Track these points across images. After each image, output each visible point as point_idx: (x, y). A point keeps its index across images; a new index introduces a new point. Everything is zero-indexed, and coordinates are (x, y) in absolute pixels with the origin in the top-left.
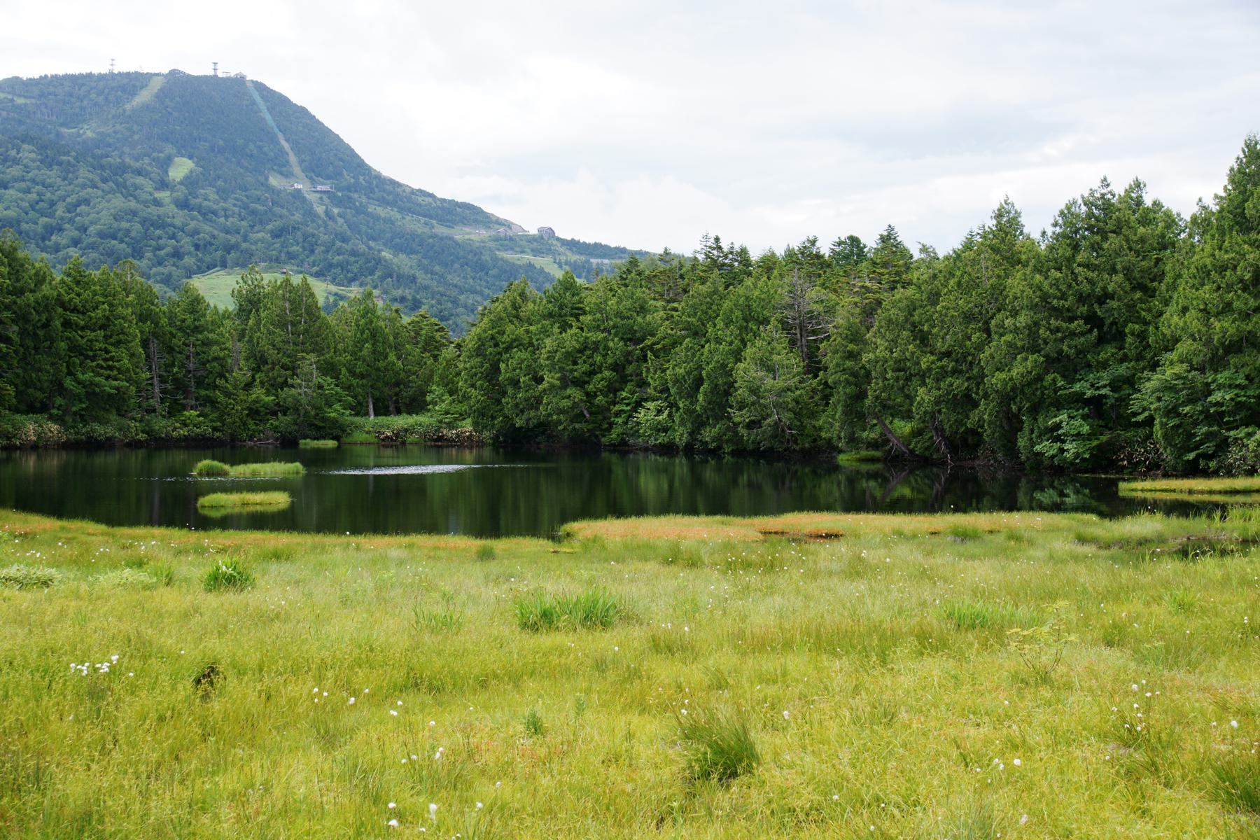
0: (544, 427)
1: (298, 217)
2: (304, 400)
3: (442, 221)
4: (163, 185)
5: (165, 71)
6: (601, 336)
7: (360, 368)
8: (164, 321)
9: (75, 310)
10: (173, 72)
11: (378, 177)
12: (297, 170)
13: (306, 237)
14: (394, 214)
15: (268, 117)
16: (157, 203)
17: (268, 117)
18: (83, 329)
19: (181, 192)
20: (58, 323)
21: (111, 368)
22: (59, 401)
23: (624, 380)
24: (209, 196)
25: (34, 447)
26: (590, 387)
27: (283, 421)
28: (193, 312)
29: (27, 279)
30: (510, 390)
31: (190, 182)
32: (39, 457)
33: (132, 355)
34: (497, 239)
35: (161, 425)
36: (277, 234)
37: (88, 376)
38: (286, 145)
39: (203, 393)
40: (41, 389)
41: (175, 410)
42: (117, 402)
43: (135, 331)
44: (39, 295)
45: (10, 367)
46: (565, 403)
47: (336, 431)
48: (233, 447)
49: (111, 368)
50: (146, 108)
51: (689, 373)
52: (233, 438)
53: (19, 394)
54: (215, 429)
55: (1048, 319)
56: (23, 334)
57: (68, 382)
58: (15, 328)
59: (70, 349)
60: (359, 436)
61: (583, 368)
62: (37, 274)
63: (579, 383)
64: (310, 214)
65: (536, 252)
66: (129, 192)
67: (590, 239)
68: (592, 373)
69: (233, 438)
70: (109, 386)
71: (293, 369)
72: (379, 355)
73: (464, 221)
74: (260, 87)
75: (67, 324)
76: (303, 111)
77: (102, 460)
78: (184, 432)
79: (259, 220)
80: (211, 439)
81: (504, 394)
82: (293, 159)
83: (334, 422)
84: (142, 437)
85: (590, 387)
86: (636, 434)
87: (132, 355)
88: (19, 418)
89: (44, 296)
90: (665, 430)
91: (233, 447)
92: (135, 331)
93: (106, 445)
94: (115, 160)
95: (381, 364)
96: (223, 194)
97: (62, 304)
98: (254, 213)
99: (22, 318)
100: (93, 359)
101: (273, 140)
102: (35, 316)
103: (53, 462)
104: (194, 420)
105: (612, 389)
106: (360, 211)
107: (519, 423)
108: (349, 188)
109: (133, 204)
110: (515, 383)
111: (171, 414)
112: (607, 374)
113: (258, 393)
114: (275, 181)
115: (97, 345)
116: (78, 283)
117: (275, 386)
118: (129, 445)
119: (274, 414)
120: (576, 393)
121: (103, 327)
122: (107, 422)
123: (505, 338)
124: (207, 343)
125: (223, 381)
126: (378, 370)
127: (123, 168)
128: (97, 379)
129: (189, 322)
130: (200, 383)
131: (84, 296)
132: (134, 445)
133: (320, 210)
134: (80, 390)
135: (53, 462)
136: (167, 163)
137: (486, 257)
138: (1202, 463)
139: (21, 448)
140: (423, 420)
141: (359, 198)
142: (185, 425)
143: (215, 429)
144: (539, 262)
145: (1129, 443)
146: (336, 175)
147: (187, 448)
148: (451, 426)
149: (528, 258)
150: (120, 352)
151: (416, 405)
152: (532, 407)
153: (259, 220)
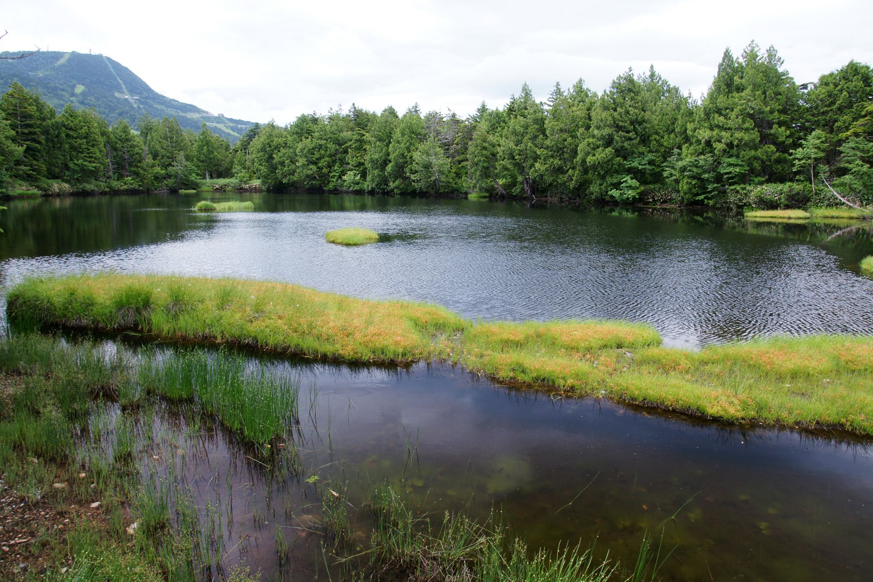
0: (293, 184)
1: (127, 108)
2: (180, 172)
3: (183, 111)
4: (73, 95)
5: (70, 51)
6: (323, 142)
7: (202, 158)
8: (112, 136)
9: (71, 129)
10: (73, 52)
11: (157, 94)
12: (125, 91)
13: (131, 116)
14: (164, 108)
15: (113, 70)
16: (72, 102)
17: (113, 70)
18: (76, 138)
19: (81, 98)
20: (64, 135)
21: (91, 157)
22: (67, 173)
23: (334, 162)
24: (91, 99)
25: (58, 195)
26: (320, 165)
27: (171, 182)
28: (125, 132)
29: (46, 111)
30: (280, 167)
31: (83, 94)
32: (61, 200)
33: (101, 151)
34: (203, 118)
35: (115, 184)
36: (120, 114)
37: (80, 161)
38: (121, 82)
39: (133, 169)
40: (58, 167)
41: (121, 177)
42: (94, 174)
43: (102, 140)
44: (53, 121)
45: (42, 156)
46: (309, 172)
47: (195, 186)
48: (148, 194)
49: (91, 157)
50: (63, 65)
51: (380, 158)
52: (148, 190)
53: (48, 169)
54: (140, 186)
55: (617, 132)
56: (47, 140)
57: (71, 165)
58: (43, 137)
59: (71, 148)
60: (204, 188)
61: (317, 155)
62: (51, 111)
63: (315, 163)
64: (132, 107)
65: (218, 122)
66: (60, 97)
67: (237, 119)
68: (320, 158)
69: (148, 190)
70: (91, 166)
71: (173, 158)
72: (211, 152)
73: (190, 111)
74: (108, 59)
75: (68, 136)
76: (126, 69)
77: (91, 201)
78: (125, 187)
79: (112, 110)
80: (139, 190)
81: (276, 169)
82: (123, 86)
83: (192, 182)
84: (107, 190)
85: (320, 165)
86: (342, 186)
87: (101, 151)
88: (50, 181)
89: (56, 122)
90: (358, 184)
91: (148, 194)
92: (102, 140)
93: (91, 194)
94: (52, 85)
95: (211, 156)
96: (97, 99)
97: (64, 126)
98: (110, 106)
99: (46, 132)
100: (82, 153)
101: (115, 79)
102: (52, 131)
103: (68, 202)
104: (130, 182)
105: (329, 166)
106: (151, 106)
107: (285, 181)
108: (146, 98)
109: (62, 102)
110: (282, 164)
111: (118, 180)
112: (327, 159)
113: (158, 169)
114: (117, 95)
115: (84, 146)
116: (71, 116)
117: (166, 166)
118: (101, 193)
119: (165, 178)
120: (314, 167)
121: (85, 138)
122: (90, 183)
123: (274, 143)
124: (133, 146)
125: (722, 118)
126: (210, 159)
127: (56, 88)
128: (86, 163)
129: (123, 136)
130: (130, 165)
131: (75, 122)
132: (103, 193)
133: (135, 106)
134: (76, 168)
135: (68, 202)
136: (74, 86)
137: (200, 124)
138: (706, 201)
139: (51, 196)
140: (233, 181)
141: (150, 102)
142: (126, 184)
143: (140, 186)
144: (219, 126)
145: (652, 191)
146: (140, 93)
147: (127, 194)
148: (245, 183)
149: (215, 124)
150: (95, 150)
151: (226, 173)
152: (290, 174)
153: (112, 110)
